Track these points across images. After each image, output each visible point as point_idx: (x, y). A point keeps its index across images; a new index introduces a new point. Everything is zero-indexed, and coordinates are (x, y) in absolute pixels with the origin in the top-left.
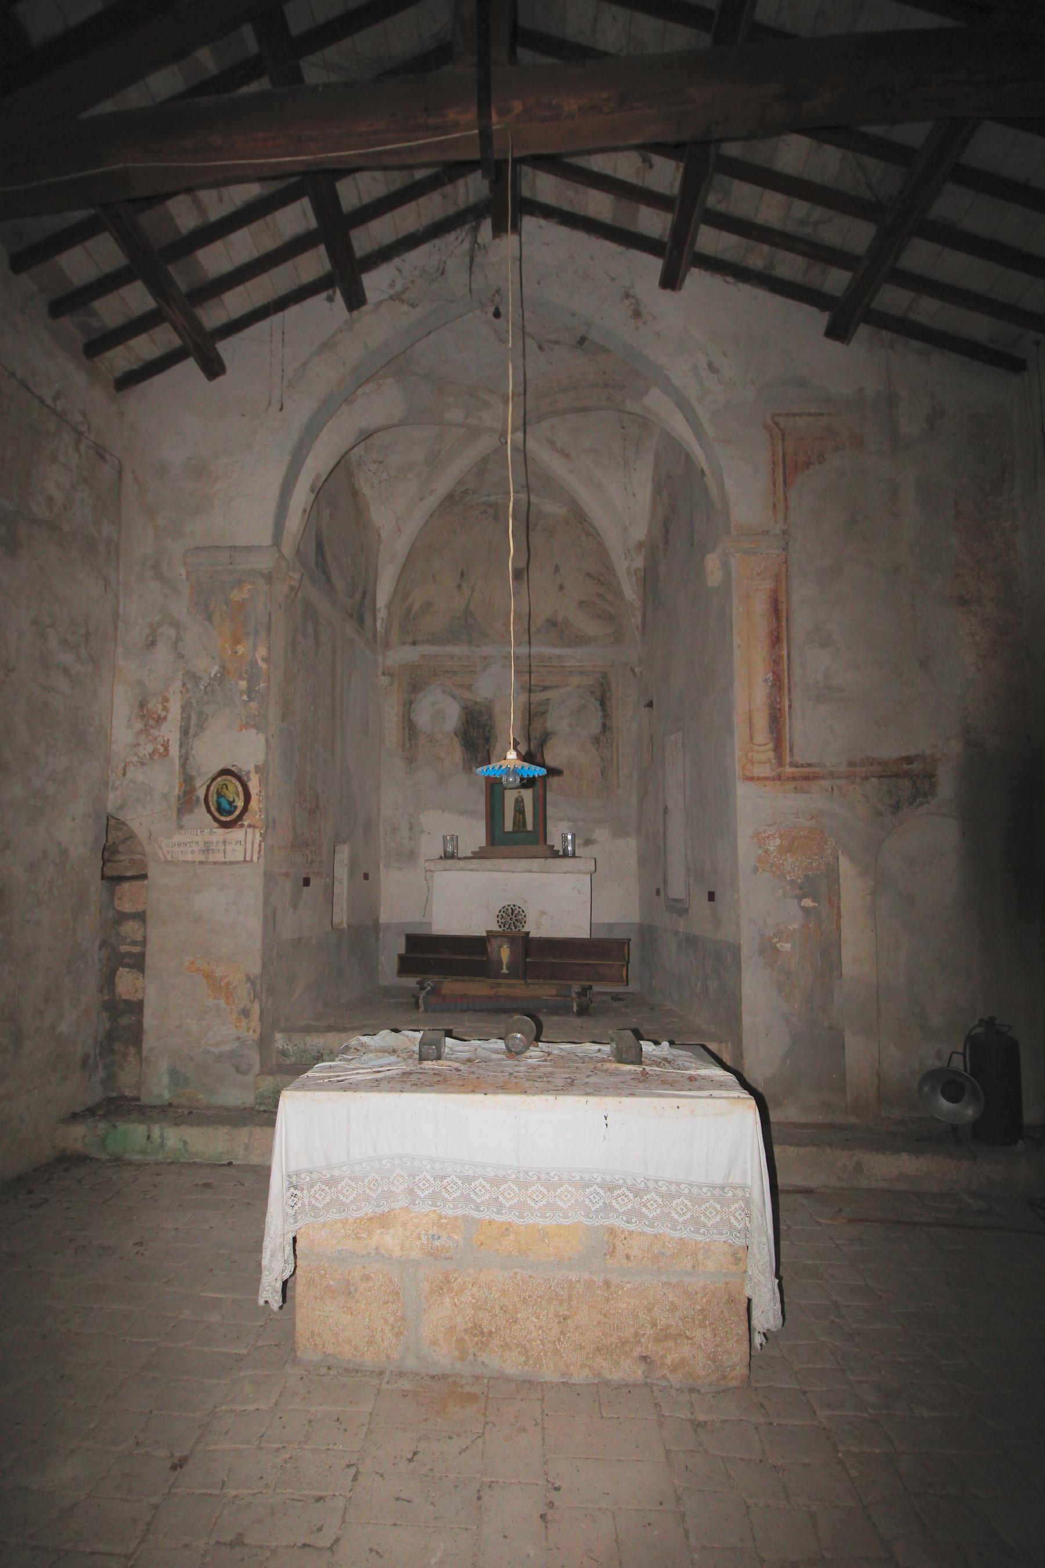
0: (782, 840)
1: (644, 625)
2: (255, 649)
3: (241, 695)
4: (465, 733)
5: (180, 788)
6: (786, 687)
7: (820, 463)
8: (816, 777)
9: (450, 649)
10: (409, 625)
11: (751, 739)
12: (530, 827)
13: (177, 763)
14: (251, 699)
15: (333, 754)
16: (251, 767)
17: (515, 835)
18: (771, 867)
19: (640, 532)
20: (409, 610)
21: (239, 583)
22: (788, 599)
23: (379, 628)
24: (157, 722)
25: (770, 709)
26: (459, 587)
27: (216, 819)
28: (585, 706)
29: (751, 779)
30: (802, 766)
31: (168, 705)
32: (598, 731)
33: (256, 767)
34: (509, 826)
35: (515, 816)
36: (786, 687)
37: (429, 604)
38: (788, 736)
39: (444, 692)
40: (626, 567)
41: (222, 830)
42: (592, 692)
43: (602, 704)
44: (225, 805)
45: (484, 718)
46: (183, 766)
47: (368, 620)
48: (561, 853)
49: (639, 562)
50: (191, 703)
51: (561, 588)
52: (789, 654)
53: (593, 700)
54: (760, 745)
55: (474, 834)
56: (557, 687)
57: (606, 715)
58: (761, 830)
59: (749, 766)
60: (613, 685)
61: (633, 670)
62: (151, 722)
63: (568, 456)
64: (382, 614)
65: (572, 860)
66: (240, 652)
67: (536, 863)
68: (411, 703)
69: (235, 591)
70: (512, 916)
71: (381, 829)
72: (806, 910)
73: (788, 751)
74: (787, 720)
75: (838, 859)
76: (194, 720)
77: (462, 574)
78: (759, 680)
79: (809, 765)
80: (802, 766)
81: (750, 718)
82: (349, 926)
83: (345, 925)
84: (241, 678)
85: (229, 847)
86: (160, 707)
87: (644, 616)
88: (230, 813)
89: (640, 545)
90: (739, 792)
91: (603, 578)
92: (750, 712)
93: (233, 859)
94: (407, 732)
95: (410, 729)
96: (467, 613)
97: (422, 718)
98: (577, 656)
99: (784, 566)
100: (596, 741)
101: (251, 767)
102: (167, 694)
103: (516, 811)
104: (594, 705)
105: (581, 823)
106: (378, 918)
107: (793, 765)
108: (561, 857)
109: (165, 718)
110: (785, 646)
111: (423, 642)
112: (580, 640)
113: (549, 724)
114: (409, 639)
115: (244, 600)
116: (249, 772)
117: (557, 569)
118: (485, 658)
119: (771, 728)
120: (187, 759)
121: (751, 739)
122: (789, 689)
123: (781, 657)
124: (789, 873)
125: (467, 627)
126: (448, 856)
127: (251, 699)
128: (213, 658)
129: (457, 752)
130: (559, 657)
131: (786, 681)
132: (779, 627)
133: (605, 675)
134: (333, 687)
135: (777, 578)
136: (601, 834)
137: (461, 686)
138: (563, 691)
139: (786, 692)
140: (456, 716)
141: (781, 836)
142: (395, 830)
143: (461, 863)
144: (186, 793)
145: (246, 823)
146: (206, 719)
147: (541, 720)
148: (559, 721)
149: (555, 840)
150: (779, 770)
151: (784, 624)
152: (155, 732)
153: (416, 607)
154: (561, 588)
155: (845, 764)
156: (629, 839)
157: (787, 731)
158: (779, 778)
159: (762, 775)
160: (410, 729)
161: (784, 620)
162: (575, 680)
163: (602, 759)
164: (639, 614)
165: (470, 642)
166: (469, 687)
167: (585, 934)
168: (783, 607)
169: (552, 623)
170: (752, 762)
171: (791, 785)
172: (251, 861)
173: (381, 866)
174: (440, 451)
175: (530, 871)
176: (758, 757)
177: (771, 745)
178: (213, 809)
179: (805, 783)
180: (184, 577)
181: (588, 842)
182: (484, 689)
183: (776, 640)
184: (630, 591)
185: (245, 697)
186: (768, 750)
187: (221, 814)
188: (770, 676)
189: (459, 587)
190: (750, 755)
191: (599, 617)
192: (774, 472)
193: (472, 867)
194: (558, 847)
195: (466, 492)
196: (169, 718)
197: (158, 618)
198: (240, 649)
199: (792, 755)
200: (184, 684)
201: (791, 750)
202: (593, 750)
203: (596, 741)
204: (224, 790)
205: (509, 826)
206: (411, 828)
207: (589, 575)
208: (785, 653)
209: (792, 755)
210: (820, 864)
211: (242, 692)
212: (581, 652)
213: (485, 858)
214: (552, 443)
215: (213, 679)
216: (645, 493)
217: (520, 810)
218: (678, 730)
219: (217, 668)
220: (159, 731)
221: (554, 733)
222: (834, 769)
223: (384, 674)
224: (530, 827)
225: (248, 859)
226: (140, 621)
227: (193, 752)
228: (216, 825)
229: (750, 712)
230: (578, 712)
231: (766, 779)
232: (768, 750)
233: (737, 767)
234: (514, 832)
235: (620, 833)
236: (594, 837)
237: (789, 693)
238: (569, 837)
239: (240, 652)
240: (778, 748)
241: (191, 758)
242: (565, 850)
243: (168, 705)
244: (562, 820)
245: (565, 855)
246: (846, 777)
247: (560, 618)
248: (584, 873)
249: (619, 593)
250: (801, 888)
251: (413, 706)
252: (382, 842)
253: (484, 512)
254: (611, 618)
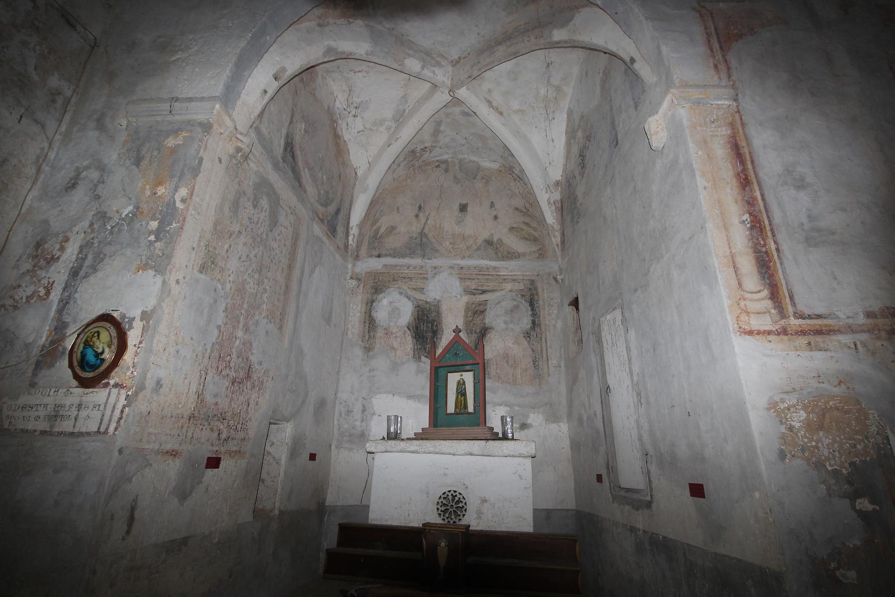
0: (808, 413)
1: (563, 242)
2: (176, 189)
3: (149, 236)
4: (417, 328)
5: (48, 337)
6: (768, 228)
7: (751, 35)
8: (830, 331)
9: (406, 261)
10: (375, 242)
11: (740, 284)
12: (471, 409)
13: (54, 308)
14: (158, 239)
15: (280, 328)
16: (137, 313)
17: (452, 421)
18: (803, 450)
19: (557, 174)
20: (377, 231)
21: (176, 132)
22: (749, 144)
23: (350, 242)
24: (48, 263)
25: (755, 252)
26: (417, 216)
27: (76, 376)
28: (517, 307)
29: (750, 333)
30: (810, 317)
31: (66, 245)
32: (529, 326)
33: (144, 313)
34: (451, 409)
35: (457, 397)
36: (768, 228)
37: (393, 228)
38: (783, 282)
39: (401, 293)
40: (547, 201)
41: (81, 390)
42: (523, 296)
43: (532, 303)
44: (91, 357)
45: (434, 314)
46: (60, 311)
47: (340, 229)
48: (500, 435)
49: (557, 196)
50: (92, 243)
51: (496, 217)
52: (762, 195)
53: (523, 302)
54: (752, 293)
55: (417, 416)
56: (493, 291)
57: (534, 313)
58: (777, 399)
59: (743, 317)
60: (540, 290)
61: (555, 279)
62: (42, 263)
63: (501, 114)
64: (354, 231)
65: (513, 442)
66: (159, 193)
67: (477, 446)
68: (373, 301)
69: (170, 139)
70: (452, 504)
71: (337, 411)
72: (862, 514)
73: (788, 300)
74: (778, 265)
75: (887, 438)
76: (88, 263)
77: (420, 208)
78: (736, 221)
79: (819, 317)
80: (810, 317)
81: (734, 262)
82: (282, 513)
83: (277, 512)
84: (153, 218)
85: (83, 413)
86: (58, 246)
87: (563, 234)
88: (94, 367)
89: (557, 183)
90: (737, 349)
91: (529, 209)
92: (733, 256)
93: (84, 430)
94: (367, 325)
95: (370, 323)
96: (422, 234)
97: (381, 314)
98: (508, 268)
99: (737, 116)
100: (527, 335)
101: (137, 313)
102: (69, 234)
103: (458, 393)
104: (525, 306)
105: (517, 408)
106: (325, 499)
107: (800, 316)
108: (500, 439)
109: (58, 258)
110: (756, 187)
111: (386, 255)
112: (511, 255)
113: (487, 321)
114: (376, 253)
115: (178, 146)
116: (134, 318)
117: (492, 205)
118: (435, 268)
119: (760, 273)
120: (67, 303)
121: (740, 284)
122: (772, 230)
123: (754, 199)
124: (828, 459)
125: (421, 245)
126: (393, 436)
127: (158, 239)
128: (130, 199)
129: (409, 343)
130: (495, 268)
131: (766, 222)
132: (745, 170)
133: (532, 282)
134: (290, 267)
135: (732, 125)
136: (535, 419)
137: (415, 289)
138: (498, 294)
139: (769, 234)
140: (409, 314)
141: (805, 408)
142: (349, 412)
143: (402, 445)
144: (52, 343)
145: (112, 382)
146: (102, 260)
147: (481, 317)
148: (495, 318)
149: (494, 420)
150: (782, 322)
151: (750, 167)
152: (42, 274)
153: (382, 230)
154: (496, 217)
155: (861, 316)
156: (562, 424)
157: (781, 277)
158: (784, 332)
159: (762, 328)
160: (370, 323)
161: (749, 163)
162: (509, 286)
163: (533, 350)
164: (558, 234)
165: (423, 256)
166: (421, 290)
167: (527, 527)
168: (745, 151)
169: (489, 242)
170: (748, 313)
171: (803, 341)
172: (106, 432)
173: (333, 447)
174: (404, 110)
175: (471, 454)
176: (753, 306)
177: (766, 293)
178: (75, 364)
179: (819, 339)
180: (124, 127)
181: (524, 426)
182: (434, 291)
183: (745, 181)
184: (550, 217)
185: (152, 238)
186: (763, 299)
187: (83, 368)
188: (746, 216)
189: (417, 216)
190: (742, 303)
191: (527, 239)
192: (709, 41)
193: (413, 448)
194: (498, 429)
195: (424, 150)
196: (62, 259)
197: (86, 163)
198: (161, 190)
199: (794, 304)
200: (92, 224)
201: (791, 298)
202: (525, 342)
203: (527, 335)
204: (95, 339)
205: (451, 409)
206: (364, 411)
207: (516, 209)
208: (758, 194)
209: (794, 304)
210: (866, 446)
211: (150, 233)
212: (512, 264)
213: (427, 439)
214: (490, 103)
215: (123, 219)
216: (561, 142)
217: (461, 392)
218: (615, 309)
219: (131, 208)
220: (47, 271)
221: (491, 328)
222: (851, 321)
223: (352, 278)
224: (471, 409)
225: (102, 430)
226: (68, 166)
227: (76, 295)
228: (75, 383)
229: (733, 256)
230: (511, 311)
231: (769, 333)
232: (763, 299)
233: (729, 317)
234: (456, 413)
235: (553, 417)
236: (529, 421)
237: (774, 236)
238: (508, 419)
239: (159, 193)
240: (775, 295)
241: (72, 302)
242: (505, 433)
243: (66, 245)
244: (500, 405)
245: (505, 438)
246: (869, 331)
247: (495, 239)
248: (525, 457)
249: (542, 221)
250: (850, 483)
251: (374, 304)
252: (336, 423)
253: (438, 166)
254: (535, 240)
